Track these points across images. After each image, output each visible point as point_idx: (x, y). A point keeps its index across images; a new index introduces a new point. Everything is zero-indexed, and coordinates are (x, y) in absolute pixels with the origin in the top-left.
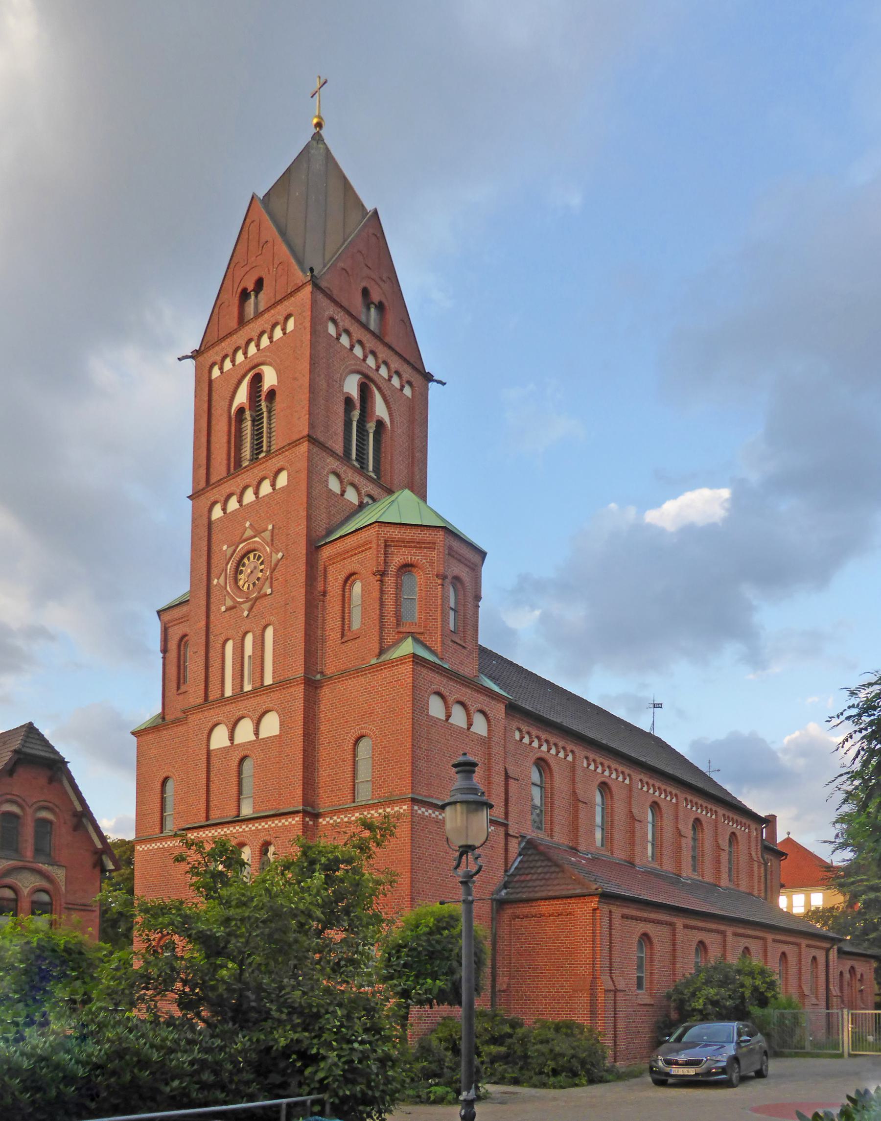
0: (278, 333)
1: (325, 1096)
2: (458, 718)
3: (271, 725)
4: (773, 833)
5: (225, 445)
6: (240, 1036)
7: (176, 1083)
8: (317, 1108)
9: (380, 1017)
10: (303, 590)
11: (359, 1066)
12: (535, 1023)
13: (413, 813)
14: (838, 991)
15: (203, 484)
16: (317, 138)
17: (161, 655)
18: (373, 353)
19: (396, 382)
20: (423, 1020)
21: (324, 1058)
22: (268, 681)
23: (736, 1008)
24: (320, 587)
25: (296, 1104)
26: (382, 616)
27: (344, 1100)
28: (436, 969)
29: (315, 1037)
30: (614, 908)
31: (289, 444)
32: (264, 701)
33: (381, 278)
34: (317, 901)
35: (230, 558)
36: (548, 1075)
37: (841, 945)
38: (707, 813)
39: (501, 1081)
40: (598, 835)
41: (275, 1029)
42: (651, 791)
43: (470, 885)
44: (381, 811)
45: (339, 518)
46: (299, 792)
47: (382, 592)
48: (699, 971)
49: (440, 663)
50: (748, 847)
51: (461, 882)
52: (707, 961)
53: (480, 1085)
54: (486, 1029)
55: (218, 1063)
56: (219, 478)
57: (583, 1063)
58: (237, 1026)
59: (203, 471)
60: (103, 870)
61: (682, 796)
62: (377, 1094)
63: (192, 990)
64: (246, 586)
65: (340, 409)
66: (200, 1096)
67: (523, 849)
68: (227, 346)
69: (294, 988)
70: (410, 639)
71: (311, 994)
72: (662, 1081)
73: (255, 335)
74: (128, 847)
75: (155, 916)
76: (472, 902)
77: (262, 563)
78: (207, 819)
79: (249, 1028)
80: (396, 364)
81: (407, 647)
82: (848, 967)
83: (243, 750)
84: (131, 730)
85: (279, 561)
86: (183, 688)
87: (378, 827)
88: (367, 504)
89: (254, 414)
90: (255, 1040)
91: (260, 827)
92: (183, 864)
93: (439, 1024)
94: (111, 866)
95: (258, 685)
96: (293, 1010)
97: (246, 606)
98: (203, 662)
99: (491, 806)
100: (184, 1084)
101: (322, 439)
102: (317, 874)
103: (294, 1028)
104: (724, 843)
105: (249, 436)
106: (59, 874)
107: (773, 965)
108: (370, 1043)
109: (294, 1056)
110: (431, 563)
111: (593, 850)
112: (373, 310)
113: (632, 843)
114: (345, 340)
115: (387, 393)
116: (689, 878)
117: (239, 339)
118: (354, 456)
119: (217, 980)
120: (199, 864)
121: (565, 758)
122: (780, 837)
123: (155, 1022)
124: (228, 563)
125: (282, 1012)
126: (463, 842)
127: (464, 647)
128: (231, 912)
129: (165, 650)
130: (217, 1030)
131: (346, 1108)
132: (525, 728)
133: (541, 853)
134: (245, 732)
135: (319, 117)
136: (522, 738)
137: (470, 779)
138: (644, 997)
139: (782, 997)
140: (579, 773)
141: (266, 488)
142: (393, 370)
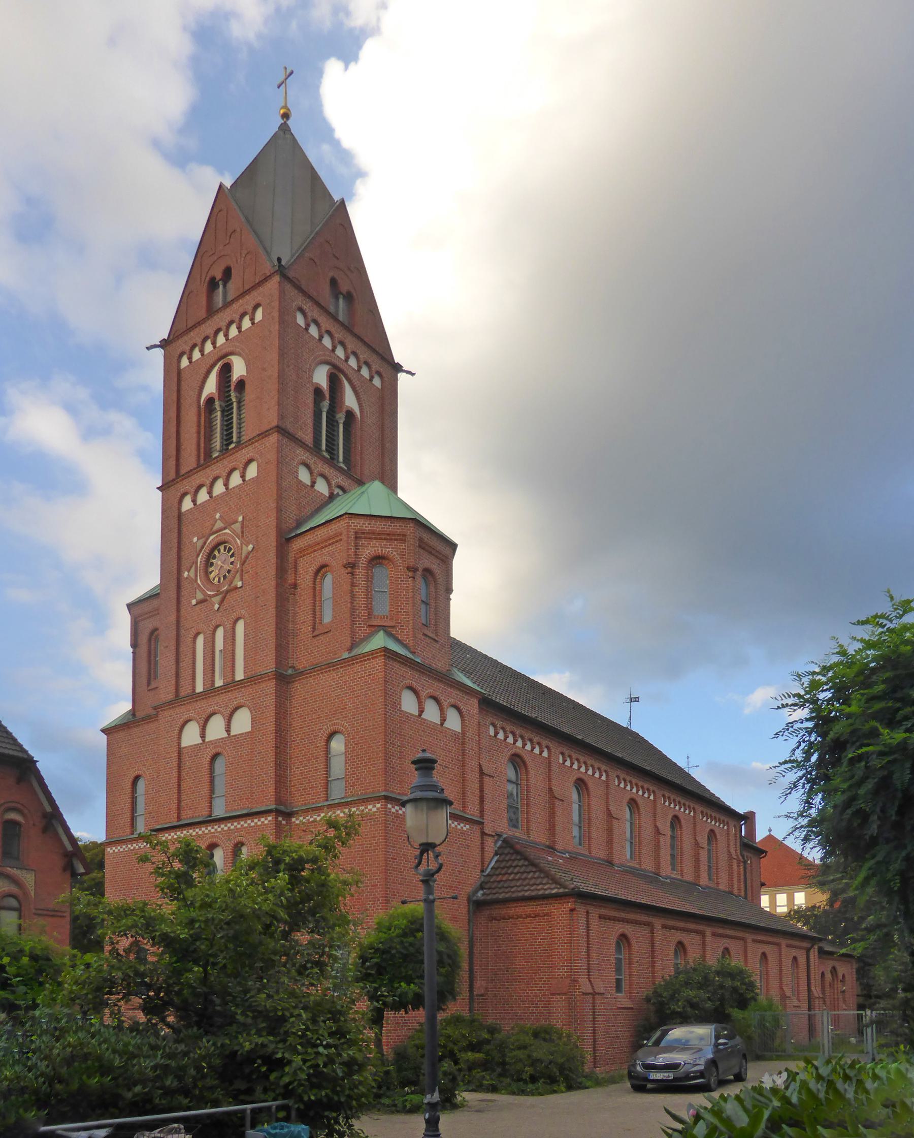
0: (246, 323)
1: (290, 1102)
2: (432, 713)
3: (243, 722)
4: (751, 831)
5: (195, 435)
6: (204, 1040)
7: (138, 1089)
8: (281, 1114)
9: (345, 1021)
10: (273, 583)
11: (325, 1070)
12: (513, 1028)
13: (386, 812)
14: (820, 992)
15: (172, 475)
16: (284, 129)
17: (131, 650)
18: (342, 343)
19: (365, 372)
20: (402, 1027)
21: (289, 1062)
22: (240, 675)
23: (716, 1010)
24: (291, 580)
25: (260, 1110)
26: (353, 610)
27: (310, 1105)
28: (410, 972)
29: (279, 1042)
30: (591, 909)
31: (259, 435)
32: (238, 697)
33: (349, 269)
34: (281, 901)
35: (201, 551)
36: (525, 1082)
37: (821, 944)
38: (685, 810)
39: (479, 1088)
40: (575, 832)
41: (240, 1033)
42: (628, 788)
43: (431, 884)
44: (347, 811)
45: (308, 510)
46: (271, 790)
47: (353, 585)
48: (678, 972)
49: (412, 657)
50: (726, 847)
51: (422, 881)
52: (686, 962)
53: (457, 1092)
54: (464, 1036)
55: (183, 1069)
56: (189, 469)
57: (562, 1068)
58: (202, 1030)
59: (173, 462)
60: (74, 874)
61: (659, 793)
62: (343, 1099)
63: (157, 994)
64: (217, 579)
65: (310, 398)
66: (164, 1102)
67: (500, 848)
68: (195, 336)
69: (259, 991)
70: (381, 633)
71: (276, 997)
72: (640, 1086)
73: (223, 324)
74: (98, 848)
75: (118, 918)
76: (433, 901)
77: (232, 556)
78: (179, 818)
79: (214, 1034)
80: (364, 354)
81: (379, 641)
82: (829, 968)
83: (214, 748)
84: (101, 727)
85: (249, 553)
86: (153, 685)
87: (343, 825)
88: (338, 495)
89: (224, 405)
90: (219, 1045)
91: (232, 827)
92: (149, 864)
93: (416, 1030)
94: (81, 870)
95: (229, 680)
96: (259, 1014)
97: (217, 599)
98: (173, 657)
99: (450, 803)
100: (146, 1090)
101: (291, 431)
102: (281, 874)
103: (259, 1033)
104: (703, 841)
105: (219, 426)
106: (28, 879)
107: (753, 968)
108: (336, 1047)
109: (259, 1061)
110: (402, 555)
111: (570, 848)
112: (341, 301)
113: (610, 841)
114: (314, 331)
115: (356, 383)
116: (666, 877)
117: (208, 328)
118: (324, 447)
119: (182, 984)
120: (163, 864)
121: (541, 754)
122: (760, 835)
123: (119, 1027)
124: (198, 555)
125: (247, 1016)
126: (424, 841)
127: (435, 640)
128: (193, 914)
129: (134, 645)
130: (182, 1035)
131: (312, 1113)
132: (499, 724)
133: (517, 852)
134: (216, 729)
135: (285, 107)
136: (496, 733)
137: (431, 776)
138: (623, 1000)
139: (762, 998)
140: (555, 768)
141: (235, 480)
142: (362, 360)
